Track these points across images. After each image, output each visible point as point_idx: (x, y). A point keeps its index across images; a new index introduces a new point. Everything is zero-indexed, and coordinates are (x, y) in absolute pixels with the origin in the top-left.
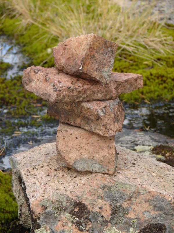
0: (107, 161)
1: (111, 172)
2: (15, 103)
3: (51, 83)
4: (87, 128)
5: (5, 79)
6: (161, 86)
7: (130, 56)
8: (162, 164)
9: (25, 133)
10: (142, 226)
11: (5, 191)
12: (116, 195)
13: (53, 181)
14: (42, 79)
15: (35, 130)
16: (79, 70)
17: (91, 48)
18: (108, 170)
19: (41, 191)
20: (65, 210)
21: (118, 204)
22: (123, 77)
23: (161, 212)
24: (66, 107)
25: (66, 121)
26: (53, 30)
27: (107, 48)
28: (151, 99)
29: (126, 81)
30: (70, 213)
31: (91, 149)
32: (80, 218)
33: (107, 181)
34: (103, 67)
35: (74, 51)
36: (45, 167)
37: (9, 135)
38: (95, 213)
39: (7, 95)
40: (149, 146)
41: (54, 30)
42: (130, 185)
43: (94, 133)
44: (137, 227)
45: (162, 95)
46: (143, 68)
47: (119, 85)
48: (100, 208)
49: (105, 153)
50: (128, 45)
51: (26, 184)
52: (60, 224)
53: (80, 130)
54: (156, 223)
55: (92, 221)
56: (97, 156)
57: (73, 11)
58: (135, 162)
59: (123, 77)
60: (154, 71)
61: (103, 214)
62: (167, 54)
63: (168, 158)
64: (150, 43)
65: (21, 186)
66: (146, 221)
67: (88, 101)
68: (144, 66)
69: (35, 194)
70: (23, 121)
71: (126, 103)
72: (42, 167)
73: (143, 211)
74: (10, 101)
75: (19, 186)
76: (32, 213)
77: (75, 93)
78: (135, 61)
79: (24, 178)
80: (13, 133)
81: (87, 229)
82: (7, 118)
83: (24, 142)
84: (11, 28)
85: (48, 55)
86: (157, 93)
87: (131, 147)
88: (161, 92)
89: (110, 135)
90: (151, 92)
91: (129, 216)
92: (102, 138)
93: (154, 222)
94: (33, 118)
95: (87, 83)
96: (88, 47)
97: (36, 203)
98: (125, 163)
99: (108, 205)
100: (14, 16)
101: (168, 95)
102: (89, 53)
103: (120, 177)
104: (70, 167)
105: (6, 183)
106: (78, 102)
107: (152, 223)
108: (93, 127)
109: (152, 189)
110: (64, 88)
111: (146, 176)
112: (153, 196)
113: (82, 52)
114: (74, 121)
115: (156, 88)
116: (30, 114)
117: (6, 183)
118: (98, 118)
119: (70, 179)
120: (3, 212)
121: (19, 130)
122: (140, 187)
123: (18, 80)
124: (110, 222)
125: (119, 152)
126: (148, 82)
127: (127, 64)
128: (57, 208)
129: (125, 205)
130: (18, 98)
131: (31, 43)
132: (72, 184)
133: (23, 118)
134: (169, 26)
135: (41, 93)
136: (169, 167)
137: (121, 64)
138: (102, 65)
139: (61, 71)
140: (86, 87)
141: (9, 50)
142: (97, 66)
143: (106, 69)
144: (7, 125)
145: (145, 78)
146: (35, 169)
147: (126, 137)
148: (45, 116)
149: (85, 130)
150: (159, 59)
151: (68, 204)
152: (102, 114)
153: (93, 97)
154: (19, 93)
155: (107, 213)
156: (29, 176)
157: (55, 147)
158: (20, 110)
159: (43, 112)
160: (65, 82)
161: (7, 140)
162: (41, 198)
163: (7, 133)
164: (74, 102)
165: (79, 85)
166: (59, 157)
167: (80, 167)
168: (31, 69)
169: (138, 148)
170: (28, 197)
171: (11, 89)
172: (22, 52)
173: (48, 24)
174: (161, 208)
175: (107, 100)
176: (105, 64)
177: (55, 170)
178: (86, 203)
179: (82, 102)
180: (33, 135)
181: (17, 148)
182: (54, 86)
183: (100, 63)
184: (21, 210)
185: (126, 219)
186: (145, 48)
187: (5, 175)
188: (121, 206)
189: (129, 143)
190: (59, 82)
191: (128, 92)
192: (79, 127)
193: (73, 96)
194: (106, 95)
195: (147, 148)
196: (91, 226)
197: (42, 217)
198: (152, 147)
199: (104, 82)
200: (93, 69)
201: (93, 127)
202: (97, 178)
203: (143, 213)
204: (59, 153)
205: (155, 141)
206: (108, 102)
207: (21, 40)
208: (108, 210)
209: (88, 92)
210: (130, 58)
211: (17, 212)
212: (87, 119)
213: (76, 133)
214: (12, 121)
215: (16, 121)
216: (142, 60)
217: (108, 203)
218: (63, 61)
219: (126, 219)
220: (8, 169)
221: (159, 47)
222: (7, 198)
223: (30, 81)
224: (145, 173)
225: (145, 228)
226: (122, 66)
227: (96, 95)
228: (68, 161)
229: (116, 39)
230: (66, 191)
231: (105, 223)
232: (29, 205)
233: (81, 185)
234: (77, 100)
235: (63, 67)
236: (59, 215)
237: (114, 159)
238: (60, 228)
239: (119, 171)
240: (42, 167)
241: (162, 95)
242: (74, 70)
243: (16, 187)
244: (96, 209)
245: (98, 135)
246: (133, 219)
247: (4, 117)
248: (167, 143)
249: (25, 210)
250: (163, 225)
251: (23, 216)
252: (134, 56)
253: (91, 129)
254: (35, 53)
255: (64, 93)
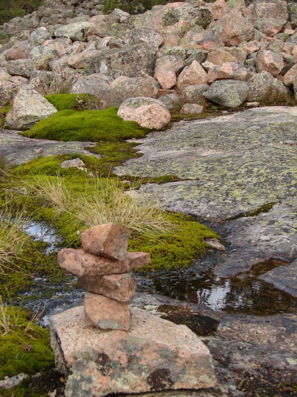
0: (124, 320)
1: (127, 329)
2: (52, 273)
3: (79, 261)
4: (108, 295)
5: (45, 255)
6: (163, 259)
7: (140, 235)
8: (166, 321)
9: (60, 297)
10: (151, 371)
11: (45, 344)
12: (131, 346)
13: (82, 337)
14: (73, 258)
15: (68, 294)
16: (101, 251)
17: (110, 234)
18: (125, 328)
19: (73, 345)
20: (91, 360)
21: (133, 354)
22: (135, 255)
23: (166, 360)
24: (91, 280)
25: (91, 290)
26: (81, 217)
27: (123, 233)
28: (156, 269)
29: (137, 258)
30: (95, 362)
31: (111, 311)
32: (103, 365)
33: (124, 336)
34: (120, 249)
35: (97, 237)
36: (75, 327)
37: (48, 299)
38: (115, 362)
39: (46, 267)
40: (156, 305)
41: (81, 216)
42: (142, 339)
43: (113, 299)
44: (148, 372)
45: (164, 265)
46: (150, 245)
47: (132, 261)
48: (119, 358)
49: (122, 314)
50: (138, 227)
51: (61, 339)
52: (87, 371)
53: (102, 297)
54: (162, 368)
55: (113, 367)
56: (116, 317)
57: (95, 202)
58: (145, 320)
59: (135, 255)
60: (157, 247)
61: (121, 362)
62: (167, 234)
63: (170, 315)
64: (155, 226)
65: (57, 341)
66: (154, 367)
67: (109, 275)
68: (150, 243)
69: (68, 347)
70: (59, 287)
71: (137, 272)
72: (74, 326)
73: (152, 358)
74: (49, 272)
75: (56, 341)
76: (66, 362)
77: (98, 269)
78: (143, 240)
79: (60, 335)
80: (51, 297)
81: (109, 374)
82: (46, 285)
83: (60, 304)
84: (49, 215)
85: (77, 236)
86: (160, 264)
87: (142, 306)
88: (164, 263)
89: (126, 301)
90: (156, 263)
91: (141, 363)
92: (120, 303)
93: (161, 367)
94: (66, 285)
95: (107, 260)
96: (108, 233)
97: (69, 354)
98: (138, 322)
99: (125, 355)
100: (51, 206)
101: (169, 265)
102: (108, 237)
103: (134, 333)
104: (95, 325)
105: (45, 338)
106: (101, 276)
107: (159, 368)
108: (112, 295)
109: (159, 342)
110: (89, 265)
111: (153, 331)
112: (159, 347)
113: (103, 237)
114: (98, 290)
115: (159, 260)
116: (64, 282)
117: (45, 338)
118: (117, 288)
119: (95, 335)
120: (43, 361)
121: (56, 295)
122: (149, 340)
123: (54, 256)
124: (127, 368)
125: (133, 313)
126: (153, 255)
127: (137, 242)
128: (86, 358)
129: (138, 355)
130: (54, 269)
131: (64, 226)
132: (97, 339)
133: (58, 285)
134: (168, 212)
135: (72, 269)
136: (171, 323)
137: (132, 242)
138: (119, 247)
139: (87, 251)
140: (106, 264)
141: (46, 232)
142: (114, 248)
143: (121, 250)
144: (47, 291)
145: (151, 253)
146: (68, 328)
147: (138, 298)
148: (76, 283)
149: (106, 297)
150: (161, 238)
151: (94, 355)
152: (119, 285)
153: (112, 272)
154: (55, 266)
155: (124, 361)
156: (64, 333)
157: (83, 310)
158: (56, 279)
159: (74, 280)
160: (91, 260)
161: (46, 303)
162: (73, 351)
163: (46, 297)
164: (98, 275)
165: (101, 263)
166: (87, 318)
167: (102, 326)
168: (65, 250)
169: (147, 307)
170: (63, 350)
171: (49, 263)
172: (57, 233)
173: (77, 212)
174: (166, 357)
175: (123, 273)
176: (121, 246)
177: (84, 328)
178: (108, 353)
179: (104, 275)
180: (66, 298)
181: (54, 309)
182: (82, 263)
183: (117, 246)
184: (57, 360)
185: (139, 366)
186: (151, 229)
187: (45, 331)
188: (135, 356)
189: (140, 303)
190: (86, 260)
191: (139, 266)
192: (102, 295)
193: (97, 271)
194: (122, 270)
195: (154, 307)
196: (112, 371)
197: (73, 366)
198: (158, 306)
199: (120, 260)
200: (112, 250)
201: (113, 295)
202: (178, 267)
203: (152, 361)
204: (86, 315)
205: (160, 301)
206: (123, 275)
207: (57, 224)
208: (125, 359)
209: (108, 268)
210: (140, 237)
211: (55, 361)
212: (108, 289)
213: (100, 299)
214: (50, 287)
215: (53, 288)
216: (149, 238)
217: (125, 353)
218: (89, 244)
219: (139, 366)
220: (47, 326)
221: (161, 228)
222: (46, 350)
223: (64, 259)
224: (153, 329)
225: (154, 373)
226: (133, 243)
227: (114, 270)
228: (94, 322)
229: (129, 223)
230: (92, 344)
231: (123, 369)
232: (63, 356)
233: (104, 339)
234: (100, 274)
235: (89, 249)
236: (87, 363)
237: (129, 319)
238: (88, 374)
239: (133, 328)
240: (74, 326)
241: (164, 265)
242: (97, 251)
243: (53, 339)
244: (116, 358)
245: (116, 301)
246: (144, 365)
247: (43, 284)
248: (169, 303)
249: (60, 359)
250: (168, 369)
251: (59, 364)
252: (143, 236)
253: (111, 296)
254: (67, 234)
255: (90, 269)
